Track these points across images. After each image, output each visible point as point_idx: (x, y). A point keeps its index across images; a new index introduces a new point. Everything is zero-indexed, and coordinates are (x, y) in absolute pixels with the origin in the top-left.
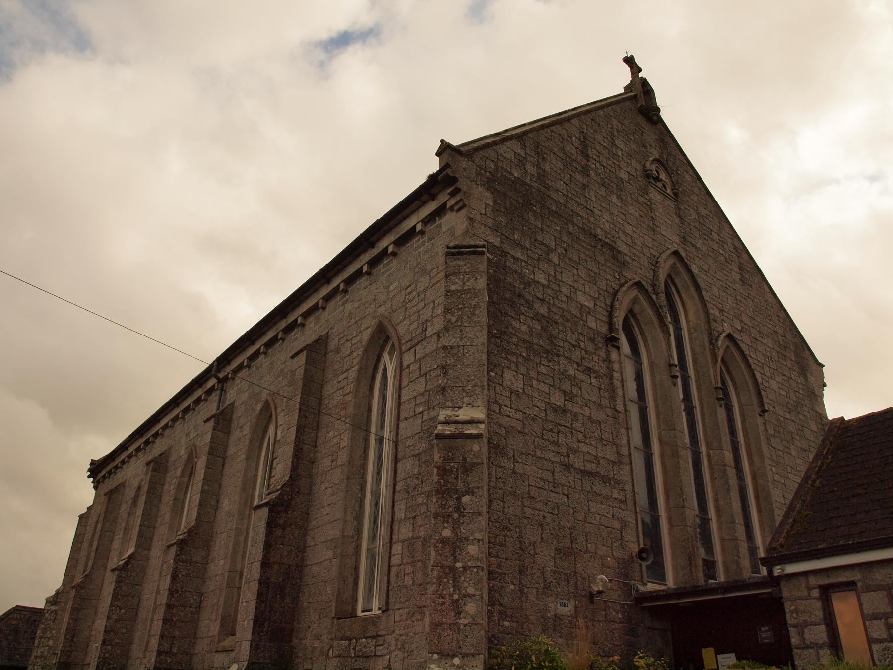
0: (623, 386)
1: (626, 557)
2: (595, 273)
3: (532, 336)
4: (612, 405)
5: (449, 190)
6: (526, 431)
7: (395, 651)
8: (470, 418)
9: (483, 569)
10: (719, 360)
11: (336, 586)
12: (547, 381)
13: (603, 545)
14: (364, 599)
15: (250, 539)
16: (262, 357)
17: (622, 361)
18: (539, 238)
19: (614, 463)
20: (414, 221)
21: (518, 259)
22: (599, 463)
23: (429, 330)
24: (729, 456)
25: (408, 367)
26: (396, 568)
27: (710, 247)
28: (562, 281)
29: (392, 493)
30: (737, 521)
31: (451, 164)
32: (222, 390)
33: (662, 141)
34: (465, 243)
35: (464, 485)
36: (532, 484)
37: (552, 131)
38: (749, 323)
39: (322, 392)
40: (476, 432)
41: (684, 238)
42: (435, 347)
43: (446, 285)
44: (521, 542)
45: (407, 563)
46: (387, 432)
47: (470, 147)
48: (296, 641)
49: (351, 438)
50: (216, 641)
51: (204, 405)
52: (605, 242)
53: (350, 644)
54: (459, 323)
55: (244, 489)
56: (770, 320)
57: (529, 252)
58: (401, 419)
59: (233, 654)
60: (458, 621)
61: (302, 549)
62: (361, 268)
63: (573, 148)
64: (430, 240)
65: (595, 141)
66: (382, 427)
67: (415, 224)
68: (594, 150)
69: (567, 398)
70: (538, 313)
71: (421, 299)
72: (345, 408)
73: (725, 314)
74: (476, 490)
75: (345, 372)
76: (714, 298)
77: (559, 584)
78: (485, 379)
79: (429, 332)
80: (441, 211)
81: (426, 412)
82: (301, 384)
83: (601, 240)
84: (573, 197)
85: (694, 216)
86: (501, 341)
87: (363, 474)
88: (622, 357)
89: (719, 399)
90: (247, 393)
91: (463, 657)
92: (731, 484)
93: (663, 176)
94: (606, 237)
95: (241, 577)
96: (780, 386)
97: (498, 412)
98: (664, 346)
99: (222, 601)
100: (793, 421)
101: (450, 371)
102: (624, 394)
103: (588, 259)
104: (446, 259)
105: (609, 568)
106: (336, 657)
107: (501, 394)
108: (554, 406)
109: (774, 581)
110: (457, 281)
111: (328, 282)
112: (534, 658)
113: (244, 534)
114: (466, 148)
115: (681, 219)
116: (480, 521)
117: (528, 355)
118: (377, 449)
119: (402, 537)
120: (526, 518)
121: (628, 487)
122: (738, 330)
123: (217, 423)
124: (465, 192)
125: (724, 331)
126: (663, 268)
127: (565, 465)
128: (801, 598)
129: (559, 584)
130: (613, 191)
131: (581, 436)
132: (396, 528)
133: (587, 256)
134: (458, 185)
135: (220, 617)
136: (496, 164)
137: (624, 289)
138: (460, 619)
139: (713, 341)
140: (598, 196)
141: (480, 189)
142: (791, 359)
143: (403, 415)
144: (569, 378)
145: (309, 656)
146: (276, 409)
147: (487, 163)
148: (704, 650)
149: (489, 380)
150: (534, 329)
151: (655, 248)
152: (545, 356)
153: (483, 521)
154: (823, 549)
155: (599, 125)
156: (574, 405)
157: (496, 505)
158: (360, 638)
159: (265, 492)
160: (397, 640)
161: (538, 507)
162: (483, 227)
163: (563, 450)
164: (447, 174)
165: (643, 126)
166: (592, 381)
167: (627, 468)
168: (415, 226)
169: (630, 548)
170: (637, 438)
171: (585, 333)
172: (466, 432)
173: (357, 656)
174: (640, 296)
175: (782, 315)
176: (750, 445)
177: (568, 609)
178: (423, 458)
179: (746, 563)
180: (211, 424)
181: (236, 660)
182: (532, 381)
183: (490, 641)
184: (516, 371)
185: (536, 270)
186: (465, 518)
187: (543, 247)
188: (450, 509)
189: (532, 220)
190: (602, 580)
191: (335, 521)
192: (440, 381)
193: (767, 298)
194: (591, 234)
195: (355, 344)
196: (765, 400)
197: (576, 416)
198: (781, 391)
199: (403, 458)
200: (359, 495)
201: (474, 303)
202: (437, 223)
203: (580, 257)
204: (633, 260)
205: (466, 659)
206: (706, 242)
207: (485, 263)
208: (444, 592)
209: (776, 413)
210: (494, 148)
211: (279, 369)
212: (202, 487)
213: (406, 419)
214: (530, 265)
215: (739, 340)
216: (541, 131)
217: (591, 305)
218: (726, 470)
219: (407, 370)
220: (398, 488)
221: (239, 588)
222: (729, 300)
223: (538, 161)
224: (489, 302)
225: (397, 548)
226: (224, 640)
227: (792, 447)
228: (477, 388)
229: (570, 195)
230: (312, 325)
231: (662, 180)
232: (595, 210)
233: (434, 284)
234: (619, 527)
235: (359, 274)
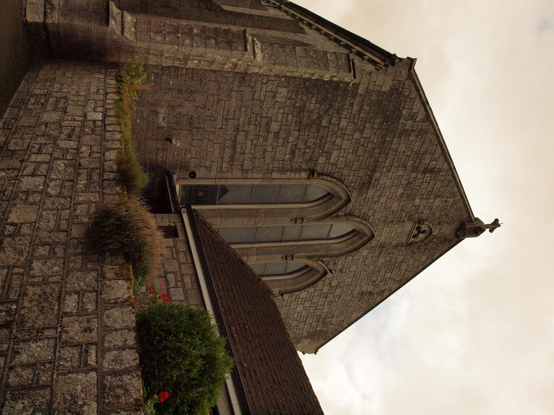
3: (309, 111)
4: (275, 169)
6: (254, 101)
21: (352, 107)
22: (241, 154)
27: (381, 269)
37: (437, 145)
41: (383, 247)
56: (340, 313)
68: (429, 178)
69: (276, 134)
73: (339, 274)
74: (218, 46)
77: (174, 117)
84: (396, 156)
85: (400, 258)
101: (282, 49)
108: (270, 123)
117: (297, 107)
124: (387, 71)
127: (238, 128)
131: (255, 142)
134: (390, 66)
137: (345, 187)
140: (401, 177)
144: (287, 138)
151: (374, 220)
155: (447, 186)
162: (367, 82)
163: (246, 128)
165: (453, 225)
166: (287, 155)
167: (240, 176)
175: (345, 324)
177: (162, 122)
187: (362, 127)
193: (354, 313)
198: (296, 314)
201: (321, 65)
203: (360, 156)
208: (166, 27)
214: (350, 116)
223: (415, 131)
234: (207, 165)
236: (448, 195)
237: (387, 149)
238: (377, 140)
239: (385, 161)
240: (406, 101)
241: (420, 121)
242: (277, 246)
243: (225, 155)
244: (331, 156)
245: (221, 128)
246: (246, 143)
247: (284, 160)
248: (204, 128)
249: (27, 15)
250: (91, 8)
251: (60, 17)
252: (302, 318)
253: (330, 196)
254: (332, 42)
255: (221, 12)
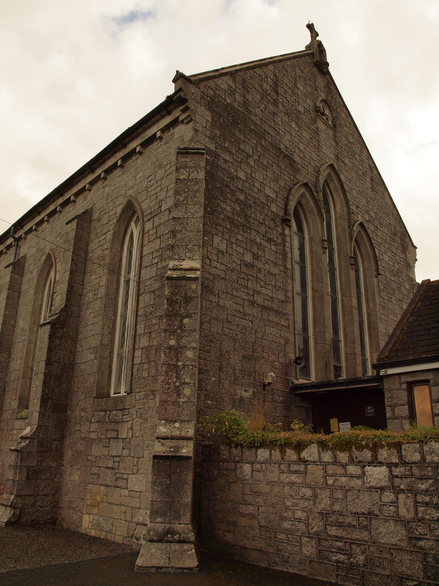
0: (291, 252)
1: (287, 362)
2: (278, 175)
3: (233, 214)
5: (181, 108)
6: (227, 278)
7: (136, 418)
8: (190, 267)
9: (196, 367)
10: (354, 239)
11: (97, 377)
12: (242, 245)
13: (273, 354)
14: (115, 385)
15: (38, 347)
16: (45, 224)
17: (292, 235)
18: (242, 147)
19: (283, 302)
20: (155, 130)
22: (273, 301)
23: (163, 206)
24: (355, 301)
25: (148, 232)
26: (137, 365)
28: (255, 178)
29: (135, 316)
30: (356, 343)
31: (183, 88)
32: (17, 246)
33: (328, 87)
34: (191, 147)
35: (185, 311)
36: (230, 313)
37: (254, 72)
38: (374, 217)
39: (87, 248)
40: (194, 276)
41: (337, 156)
42: (167, 218)
43: (177, 175)
44: (220, 351)
45: (145, 363)
46: (133, 276)
47: (197, 78)
48: (69, 412)
49: (108, 280)
50: (16, 412)
51: (4, 257)
52: (285, 154)
53: (105, 414)
54: (185, 202)
55: (33, 314)
57: (235, 156)
58: (142, 267)
59: (27, 421)
60: (179, 400)
61: (73, 353)
62: (117, 162)
63: (269, 86)
64: (166, 143)
65: (283, 82)
66: (129, 272)
67: (155, 132)
68: (282, 89)
69: (255, 258)
70: (239, 199)
71: (158, 185)
72: (104, 259)
73: (360, 209)
74: (193, 315)
75: (104, 234)
76: (354, 198)
77: (244, 378)
78: (201, 241)
79: (164, 208)
80: (174, 123)
81: (160, 263)
82: (73, 242)
83: (283, 152)
85: (345, 142)
86: (213, 217)
87: (116, 304)
88: (292, 233)
89: (351, 265)
90: (35, 249)
91: (181, 422)
92: (354, 319)
93: (327, 112)
94: (287, 151)
95: (32, 372)
96: (390, 259)
97: (209, 264)
98: (320, 227)
99: (19, 387)
100: (395, 282)
101: (178, 235)
102: (292, 257)
103: (274, 165)
104: (177, 157)
105: (276, 368)
106: (97, 422)
107: (211, 252)
108: (246, 262)
109: (380, 379)
110: (184, 172)
111: (93, 171)
112: (227, 423)
113: (34, 344)
114: (195, 78)
115: (337, 143)
116: (195, 335)
117: (230, 227)
118: (125, 287)
119: (142, 345)
120: (225, 335)
121: (291, 318)
122: (367, 221)
123: (14, 268)
125: (358, 221)
126: (323, 175)
127: (251, 302)
128: (395, 389)
129: (244, 378)
130: (293, 119)
131: (262, 283)
132: (138, 340)
133: (273, 162)
134: (188, 104)
135: (18, 397)
136: (215, 92)
137: (296, 187)
138: (180, 398)
139: (351, 226)
141: (203, 109)
142: (398, 243)
143: (144, 264)
145: (79, 422)
146: (55, 260)
147: (209, 91)
148: (331, 420)
149: (204, 242)
150: (235, 210)
151: (318, 161)
152: (242, 228)
153: (196, 335)
154: (411, 360)
155: (287, 71)
156: (260, 263)
157: (205, 326)
158: (113, 410)
159: (48, 315)
160: (137, 412)
161: (233, 328)
162: (204, 136)
163: (251, 292)
164: (180, 95)
165: (316, 75)
168: (156, 134)
169: (290, 357)
170: (298, 287)
171: (269, 215)
172: (187, 276)
173: (110, 422)
174: (306, 193)
175: (395, 213)
176: (368, 295)
177: (249, 394)
178: (157, 293)
179: (360, 368)
180: (10, 269)
181: (29, 424)
182: (232, 245)
183: (198, 412)
184: (222, 238)
185: (239, 169)
186: (185, 333)
188: (175, 327)
189: (238, 134)
190: (271, 376)
191: (96, 334)
192: (170, 242)
193: (386, 201)
194: (276, 147)
195: (111, 216)
196: (380, 267)
197: (260, 269)
199: (143, 293)
200: (113, 318)
201: (195, 188)
202: (171, 131)
203: (268, 163)
204: (303, 168)
205: (183, 424)
206: (352, 160)
207: (204, 161)
208: (170, 381)
209: (386, 276)
210: (214, 80)
211: (58, 232)
212: (5, 311)
213: (146, 267)
214: (235, 165)
215: (367, 227)
216: (248, 72)
217: (274, 197)
218: (352, 310)
219: (147, 234)
220: (140, 312)
221: (31, 379)
222: (363, 201)
223: (244, 92)
224: (205, 189)
225: (138, 353)
226: (21, 411)
227: (393, 298)
228: (195, 247)
229: (264, 119)
230: (81, 202)
231: (326, 115)
232: (281, 131)
233: (168, 175)
234: (284, 343)
235: (114, 167)
236: (294, 73)
237: (261, 130)
238: (255, 139)
239: (271, 135)
240: (219, 95)
241: (235, 84)
242: (340, 273)
243: (275, 320)
244: (270, 196)
245: (252, 322)
246: (264, 294)
247: (276, 252)
248: (252, 343)
249: (189, 566)
250: (164, 480)
251: (181, 522)
252: (392, 257)
253: (299, 207)
254: (109, 177)
255: (66, 311)
